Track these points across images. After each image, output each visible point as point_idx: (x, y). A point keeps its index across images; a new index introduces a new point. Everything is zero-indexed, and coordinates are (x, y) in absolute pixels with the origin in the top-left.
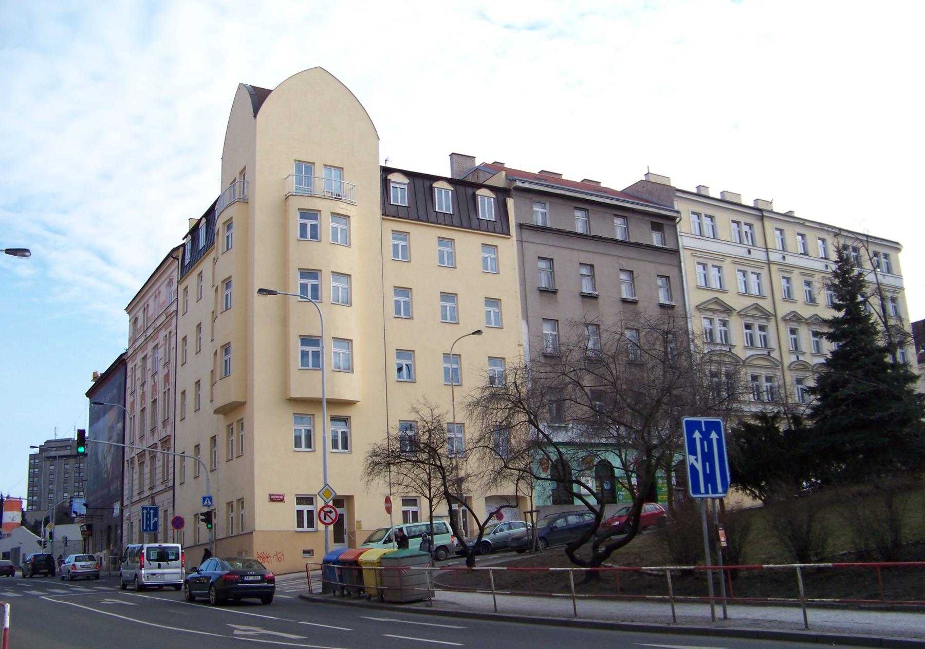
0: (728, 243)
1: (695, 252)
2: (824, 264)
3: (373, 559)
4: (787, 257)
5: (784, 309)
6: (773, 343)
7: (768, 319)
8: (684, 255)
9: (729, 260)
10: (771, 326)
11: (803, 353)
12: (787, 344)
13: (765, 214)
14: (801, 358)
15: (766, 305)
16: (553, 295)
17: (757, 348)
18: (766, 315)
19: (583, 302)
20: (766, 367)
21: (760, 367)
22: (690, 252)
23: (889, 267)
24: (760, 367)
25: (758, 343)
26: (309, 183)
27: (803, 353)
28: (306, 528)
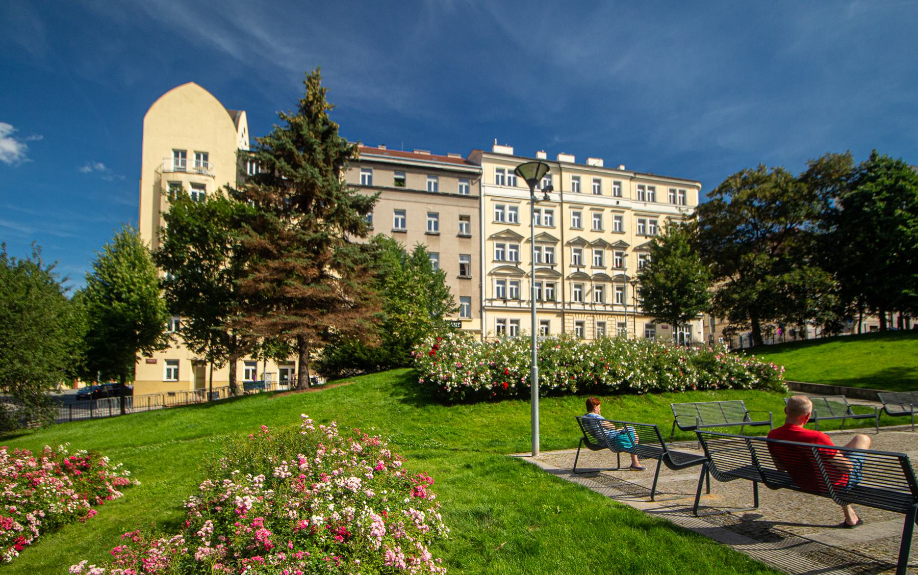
0: (588, 195)
1: (494, 198)
2: (616, 201)
3: (869, 373)
4: (620, 202)
5: (570, 236)
6: (558, 259)
7: (555, 244)
8: (486, 201)
9: (587, 208)
10: (558, 248)
11: (584, 267)
12: (568, 260)
13: (562, 166)
14: (581, 270)
15: (555, 233)
16: (404, 234)
17: (543, 264)
18: (554, 241)
19: (460, 241)
20: (510, 275)
21: (505, 275)
22: (490, 198)
23: (446, 174)
24: (505, 275)
25: (544, 260)
26: (184, 163)
27: (584, 267)
28: (173, 379)
